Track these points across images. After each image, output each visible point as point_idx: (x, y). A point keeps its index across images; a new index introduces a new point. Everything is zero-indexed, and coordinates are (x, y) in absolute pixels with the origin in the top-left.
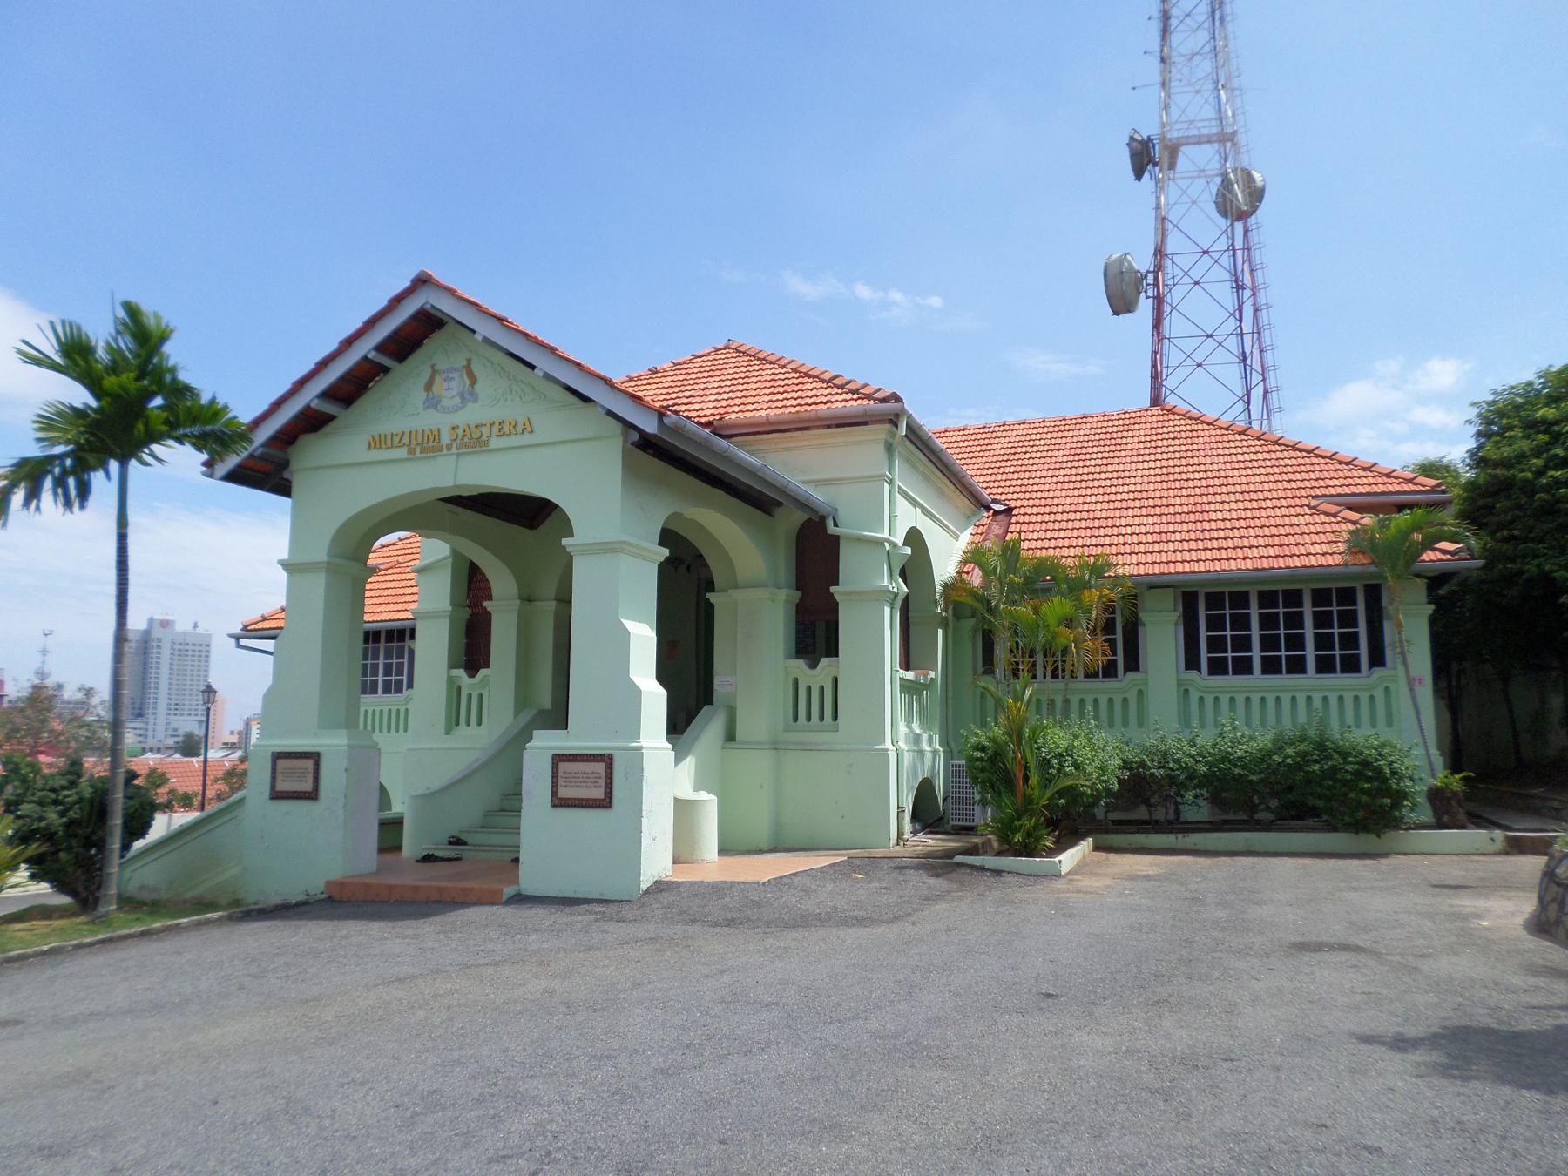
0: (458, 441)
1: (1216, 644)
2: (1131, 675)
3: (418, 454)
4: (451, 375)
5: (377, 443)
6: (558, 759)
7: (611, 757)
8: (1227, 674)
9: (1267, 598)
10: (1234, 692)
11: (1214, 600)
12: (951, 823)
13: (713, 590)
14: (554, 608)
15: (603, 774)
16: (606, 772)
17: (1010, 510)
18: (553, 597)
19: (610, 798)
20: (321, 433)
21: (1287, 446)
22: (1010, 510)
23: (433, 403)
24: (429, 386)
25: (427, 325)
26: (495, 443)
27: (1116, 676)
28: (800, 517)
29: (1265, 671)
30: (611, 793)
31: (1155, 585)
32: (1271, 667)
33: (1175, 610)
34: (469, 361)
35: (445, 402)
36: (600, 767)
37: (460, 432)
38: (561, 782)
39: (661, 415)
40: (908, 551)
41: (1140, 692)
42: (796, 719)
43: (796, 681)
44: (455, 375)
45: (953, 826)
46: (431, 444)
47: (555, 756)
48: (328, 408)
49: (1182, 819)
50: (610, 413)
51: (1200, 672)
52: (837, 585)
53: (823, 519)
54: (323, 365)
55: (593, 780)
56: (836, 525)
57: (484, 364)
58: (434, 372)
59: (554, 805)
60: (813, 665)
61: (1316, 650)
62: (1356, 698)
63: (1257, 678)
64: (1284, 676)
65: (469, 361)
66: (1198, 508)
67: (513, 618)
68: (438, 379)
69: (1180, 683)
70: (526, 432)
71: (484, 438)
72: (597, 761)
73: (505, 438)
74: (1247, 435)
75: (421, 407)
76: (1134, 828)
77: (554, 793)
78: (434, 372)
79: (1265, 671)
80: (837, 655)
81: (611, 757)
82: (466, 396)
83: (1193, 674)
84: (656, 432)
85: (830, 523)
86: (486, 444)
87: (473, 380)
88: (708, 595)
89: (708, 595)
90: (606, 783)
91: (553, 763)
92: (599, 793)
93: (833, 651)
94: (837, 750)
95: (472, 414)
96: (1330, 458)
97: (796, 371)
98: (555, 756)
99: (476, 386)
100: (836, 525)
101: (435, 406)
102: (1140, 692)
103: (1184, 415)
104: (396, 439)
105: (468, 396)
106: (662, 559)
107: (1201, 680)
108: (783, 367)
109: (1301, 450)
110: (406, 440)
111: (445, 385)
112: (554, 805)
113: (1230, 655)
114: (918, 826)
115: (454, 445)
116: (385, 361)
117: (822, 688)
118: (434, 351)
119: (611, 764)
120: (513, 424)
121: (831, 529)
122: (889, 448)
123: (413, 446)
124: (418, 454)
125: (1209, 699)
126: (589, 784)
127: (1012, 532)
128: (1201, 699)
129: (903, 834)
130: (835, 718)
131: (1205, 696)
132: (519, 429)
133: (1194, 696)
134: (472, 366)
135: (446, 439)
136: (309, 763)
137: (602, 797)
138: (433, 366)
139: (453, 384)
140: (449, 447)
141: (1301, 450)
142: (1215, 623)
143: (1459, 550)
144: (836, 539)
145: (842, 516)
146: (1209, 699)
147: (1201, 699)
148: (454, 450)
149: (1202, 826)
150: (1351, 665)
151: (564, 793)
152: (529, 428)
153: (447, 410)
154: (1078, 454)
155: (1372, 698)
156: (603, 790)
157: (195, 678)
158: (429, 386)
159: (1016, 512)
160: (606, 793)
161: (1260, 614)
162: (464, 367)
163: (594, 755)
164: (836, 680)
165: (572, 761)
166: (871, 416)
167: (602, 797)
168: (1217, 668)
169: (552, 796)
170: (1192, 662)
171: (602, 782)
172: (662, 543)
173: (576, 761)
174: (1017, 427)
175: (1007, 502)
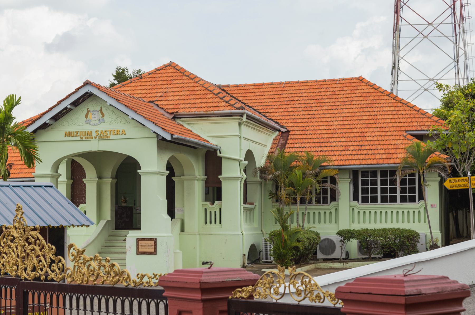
0: (99, 136)
1: (365, 191)
2: (333, 203)
3: (84, 139)
4: (95, 113)
5: (68, 134)
6: (138, 240)
7: (156, 239)
8: (368, 202)
9: (384, 173)
10: (365, 209)
11: (365, 173)
12: (262, 260)
13: (174, 176)
14: (111, 181)
15: (154, 245)
16: (155, 244)
17: (288, 132)
18: (110, 177)
19: (156, 251)
20: (46, 129)
21: (404, 104)
22: (288, 132)
23: (88, 122)
24: (86, 116)
25: (88, 96)
26: (112, 137)
27: (327, 203)
28: (205, 150)
29: (382, 201)
30: (156, 250)
31: (341, 170)
32: (384, 200)
33: (349, 178)
34: (101, 108)
35: (93, 122)
36: (153, 242)
37: (99, 133)
38: (140, 247)
39: (172, 135)
40: (246, 162)
41: (336, 209)
42: (206, 223)
43: (206, 209)
44: (97, 113)
45: (263, 261)
46: (88, 136)
47: (137, 239)
48: (51, 122)
49: (350, 258)
50: (154, 132)
51: (358, 202)
52: (221, 175)
53: (215, 151)
54: (51, 109)
55: (150, 246)
56: (220, 153)
57: (107, 110)
58: (88, 111)
59: (137, 254)
60: (213, 204)
61: (377, 202)
62: (414, 212)
63: (379, 205)
64: (389, 203)
65: (101, 108)
66: (363, 135)
67: (95, 185)
68: (90, 114)
69: (350, 206)
70: (123, 134)
71: (108, 135)
72: (152, 240)
73: (116, 136)
74: (389, 97)
75: (84, 123)
76: (331, 261)
77: (137, 250)
78: (88, 111)
79: (382, 201)
80: (221, 200)
81: (156, 239)
82: (101, 120)
83: (355, 203)
84: (170, 140)
85: (218, 152)
86: (109, 137)
87: (103, 115)
88: (172, 178)
89: (172, 178)
90: (155, 247)
91: (137, 241)
92: (153, 250)
93: (219, 199)
94: (212, 234)
95: (102, 127)
96: (418, 111)
97: (202, 86)
98: (137, 239)
99: (104, 117)
100: (220, 153)
101: (89, 123)
102: (336, 209)
103: (366, 84)
104: (75, 133)
105: (101, 121)
106: (167, 174)
107: (359, 205)
108: (197, 82)
109: (408, 106)
110: (79, 134)
111: (93, 116)
112: (137, 254)
113: (389, 186)
114: (249, 262)
115: (97, 137)
116: (72, 107)
117: (215, 212)
118: (90, 106)
119: (156, 241)
120: (119, 131)
121: (219, 154)
122: (240, 124)
123: (82, 136)
124: (84, 139)
125: (362, 212)
126: (149, 247)
127: (291, 135)
128: (359, 212)
129: (245, 264)
130: (220, 223)
131: (360, 211)
132: (121, 133)
133: (356, 211)
134: (102, 110)
135: (94, 135)
136: (153, 242)
137: (154, 251)
138: (88, 109)
139: (95, 116)
140: (95, 138)
141: (408, 106)
142: (364, 183)
143: (448, 158)
144: (221, 158)
145: (223, 149)
146: (362, 212)
147: (359, 212)
148: (97, 139)
149: (355, 260)
150: (412, 200)
151: (140, 250)
152: (123, 133)
153: (94, 125)
154: (319, 102)
155: (419, 212)
156: (154, 249)
157: (267, 244)
158: (86, 116)
159: (290, 133)
160: (155, 250)
161: (381, 179)
162: (99, 110)
163: (150, 238)
164: (220, 209)
165: (143, 240)
166: (233, 114)
167: (154, 251)
168: (365, 200)
169: (137, 251)
170: (355, 198)
171: (153, 247)
172: (167, 169)
173: (145, 240)
174: (295, 85)
175: (287, 128)
